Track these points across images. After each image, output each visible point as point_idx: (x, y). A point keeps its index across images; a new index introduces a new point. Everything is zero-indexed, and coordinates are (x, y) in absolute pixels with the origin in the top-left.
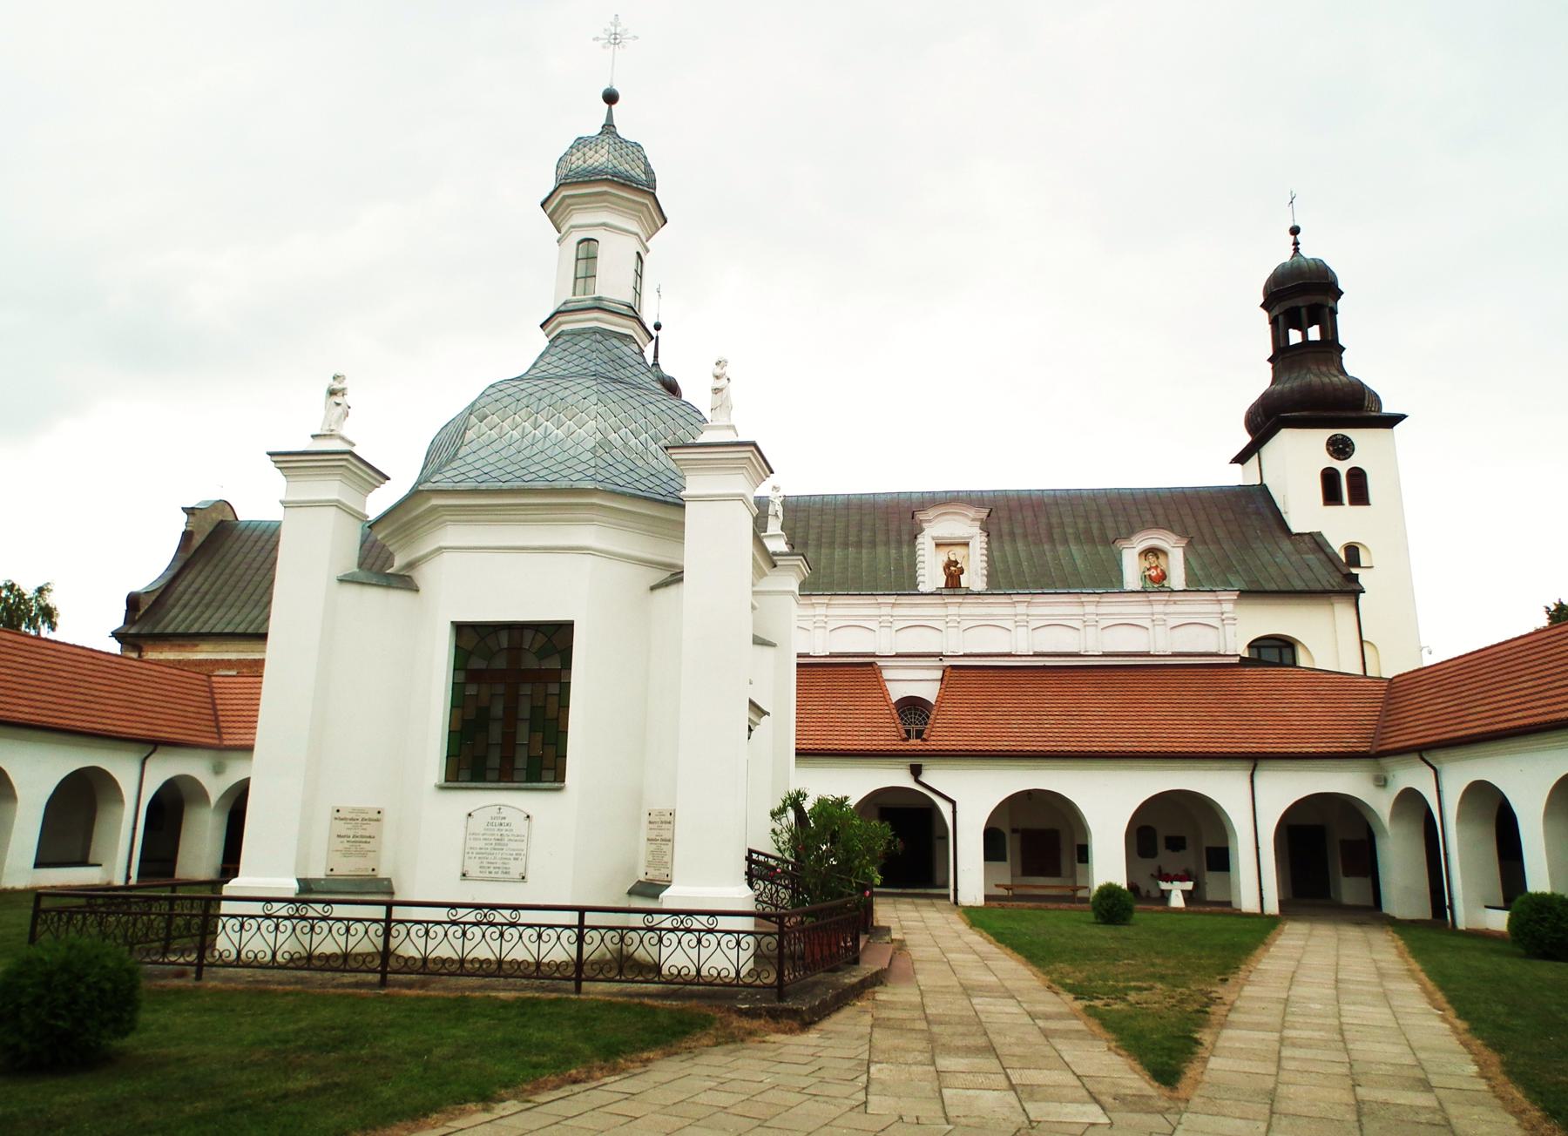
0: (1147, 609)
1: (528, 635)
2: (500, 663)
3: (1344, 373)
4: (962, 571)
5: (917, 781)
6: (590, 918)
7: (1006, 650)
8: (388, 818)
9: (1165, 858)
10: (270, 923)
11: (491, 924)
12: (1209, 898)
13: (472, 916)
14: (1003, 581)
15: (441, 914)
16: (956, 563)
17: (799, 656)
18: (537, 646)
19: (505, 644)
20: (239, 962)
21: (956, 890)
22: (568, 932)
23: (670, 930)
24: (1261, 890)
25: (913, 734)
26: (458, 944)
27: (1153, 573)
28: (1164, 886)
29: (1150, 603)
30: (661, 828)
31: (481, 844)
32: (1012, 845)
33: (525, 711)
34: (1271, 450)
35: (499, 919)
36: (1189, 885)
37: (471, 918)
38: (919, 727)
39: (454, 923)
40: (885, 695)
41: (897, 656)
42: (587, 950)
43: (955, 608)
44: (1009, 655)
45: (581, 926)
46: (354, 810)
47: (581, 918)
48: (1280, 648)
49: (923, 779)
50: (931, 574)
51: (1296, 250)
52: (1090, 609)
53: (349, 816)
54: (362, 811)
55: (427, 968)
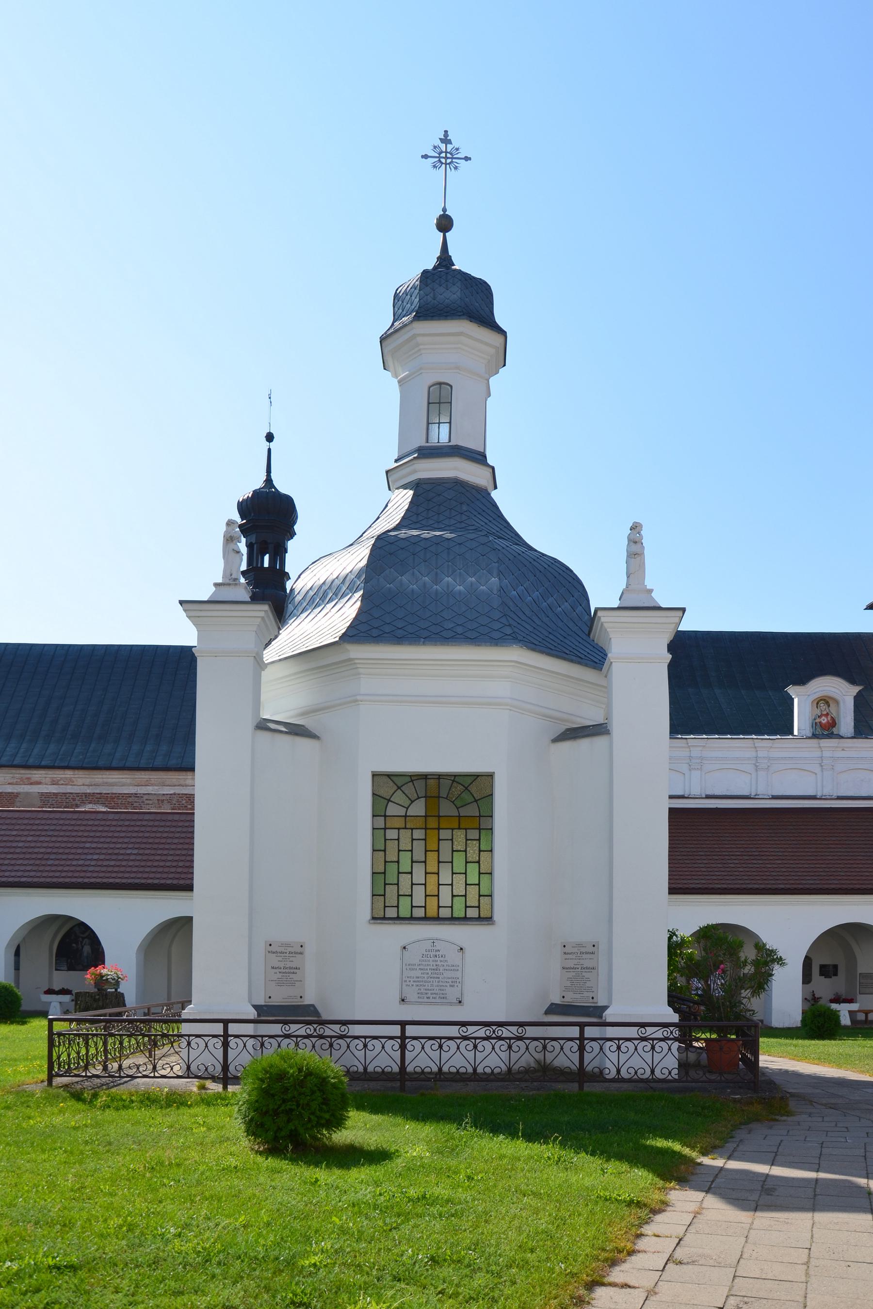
7: (680, 793)
8: (309, 950)
11: (500, 1038)
13: (482, 1032)
15: (453, 1031)
17: (671, 797)
23: (484, 1039)
26: (504, 1056)
27: (824, 720)
30: (582, 959)
31: (418, 973)
37: (659, 1035)
39: (465, 1038)
42: (587, 1057)
44: (814, 798)
46: (283, 945)
47: (582, 1032)
53: (279, 949)
54: (288, 945)
55: (422, 1076)
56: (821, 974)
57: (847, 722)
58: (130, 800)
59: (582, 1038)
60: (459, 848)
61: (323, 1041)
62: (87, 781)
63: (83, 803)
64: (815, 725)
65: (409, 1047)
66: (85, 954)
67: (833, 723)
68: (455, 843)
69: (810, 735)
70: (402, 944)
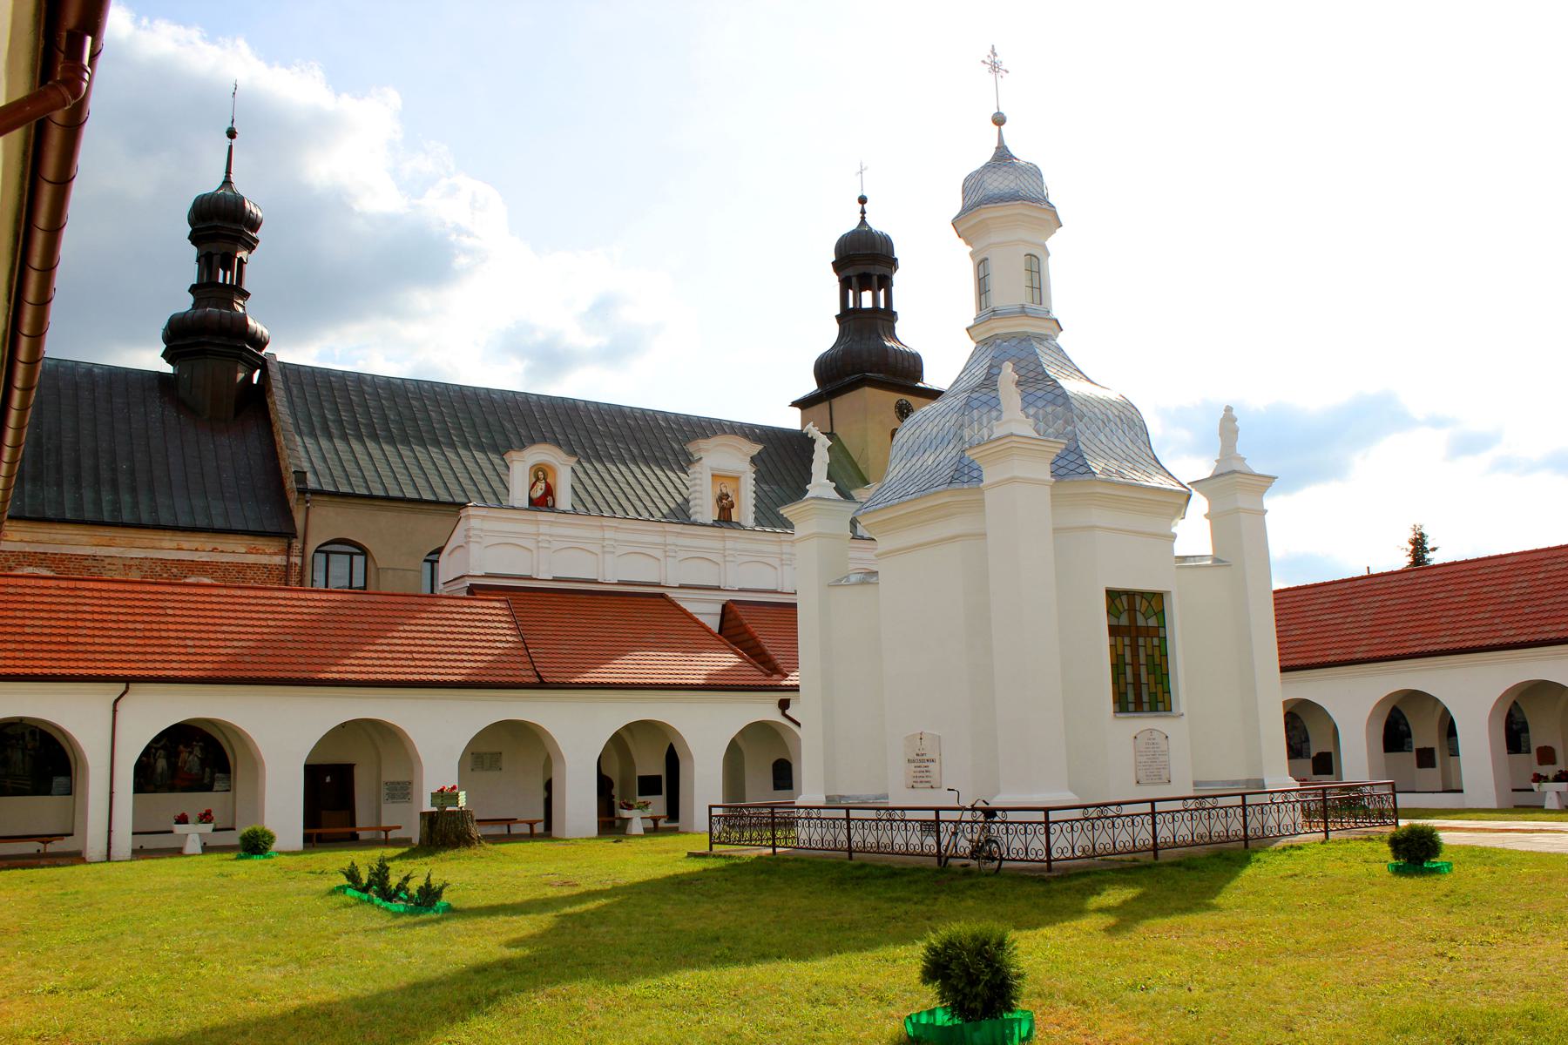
3: (894, 337)
10: (1187, 814)
20: (1175, 845)
24: (110, 831)
33: (1142, 659)
43: (730, 541)
44: (775, 592)
45: (1047, 822)
48: (351, 554)
51: (863, 218)
56: (1431, 750)
57: (745, 510)
58: (86, 563)
59: (1047, 822)
62: (27, 537)
63: (20, 565)
66: (159, 770)
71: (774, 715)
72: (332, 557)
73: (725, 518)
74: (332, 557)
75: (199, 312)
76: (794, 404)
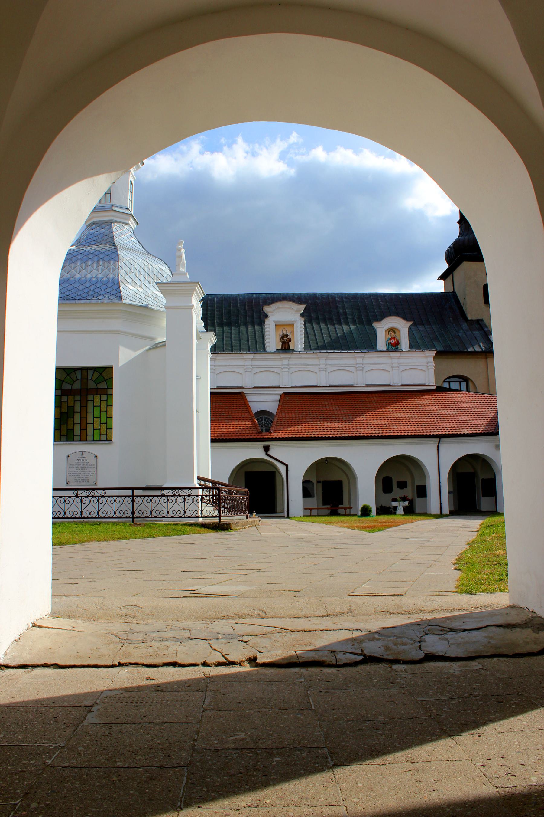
0: (389, 361)
1: (90, 373)
2: (77, 385)
4: (290, 340)
5: (267, 454)
6: (137, 493)
9: (397, 492)
11: (93, 496)
12: (417, 512)
13: (85, 493)
14: (313, 345)
16: (287, 335)
18: (94, 379)
19: (79, 377)
21: (288, 511)
22: (127, 498)
23: (172, 496)
24: (441, 503)
25: (264, 431)
27: (393, 341)
28: (394, 504)
29: (391, 357)
31: (75, 469)
32: (317, 490)
34: (459, 273)
35: (96, 494)
36: (407, 503)
37: (171, 494)
38: (267, 428)
39: (163, 496)
40: (248, 409)
41: (255, 387)
43: (286, 359)
44: (316, 386)
47: (133, 493)
48: (460, 382)
49: (269, 453)
50: (272, 341)
52: (359, 361)
60: (97, 405)
61: (94, 498)
64: (388, 344)
65: (136, 501)
67: (398, 343)
68: (95, 402)
69: (385, 350)
70: (68, 454)
71: (262, 455)
72: (451, 383)
73: (286, 346)
74: (451, 383)
75: (463, 238)
76: (441, 278)
